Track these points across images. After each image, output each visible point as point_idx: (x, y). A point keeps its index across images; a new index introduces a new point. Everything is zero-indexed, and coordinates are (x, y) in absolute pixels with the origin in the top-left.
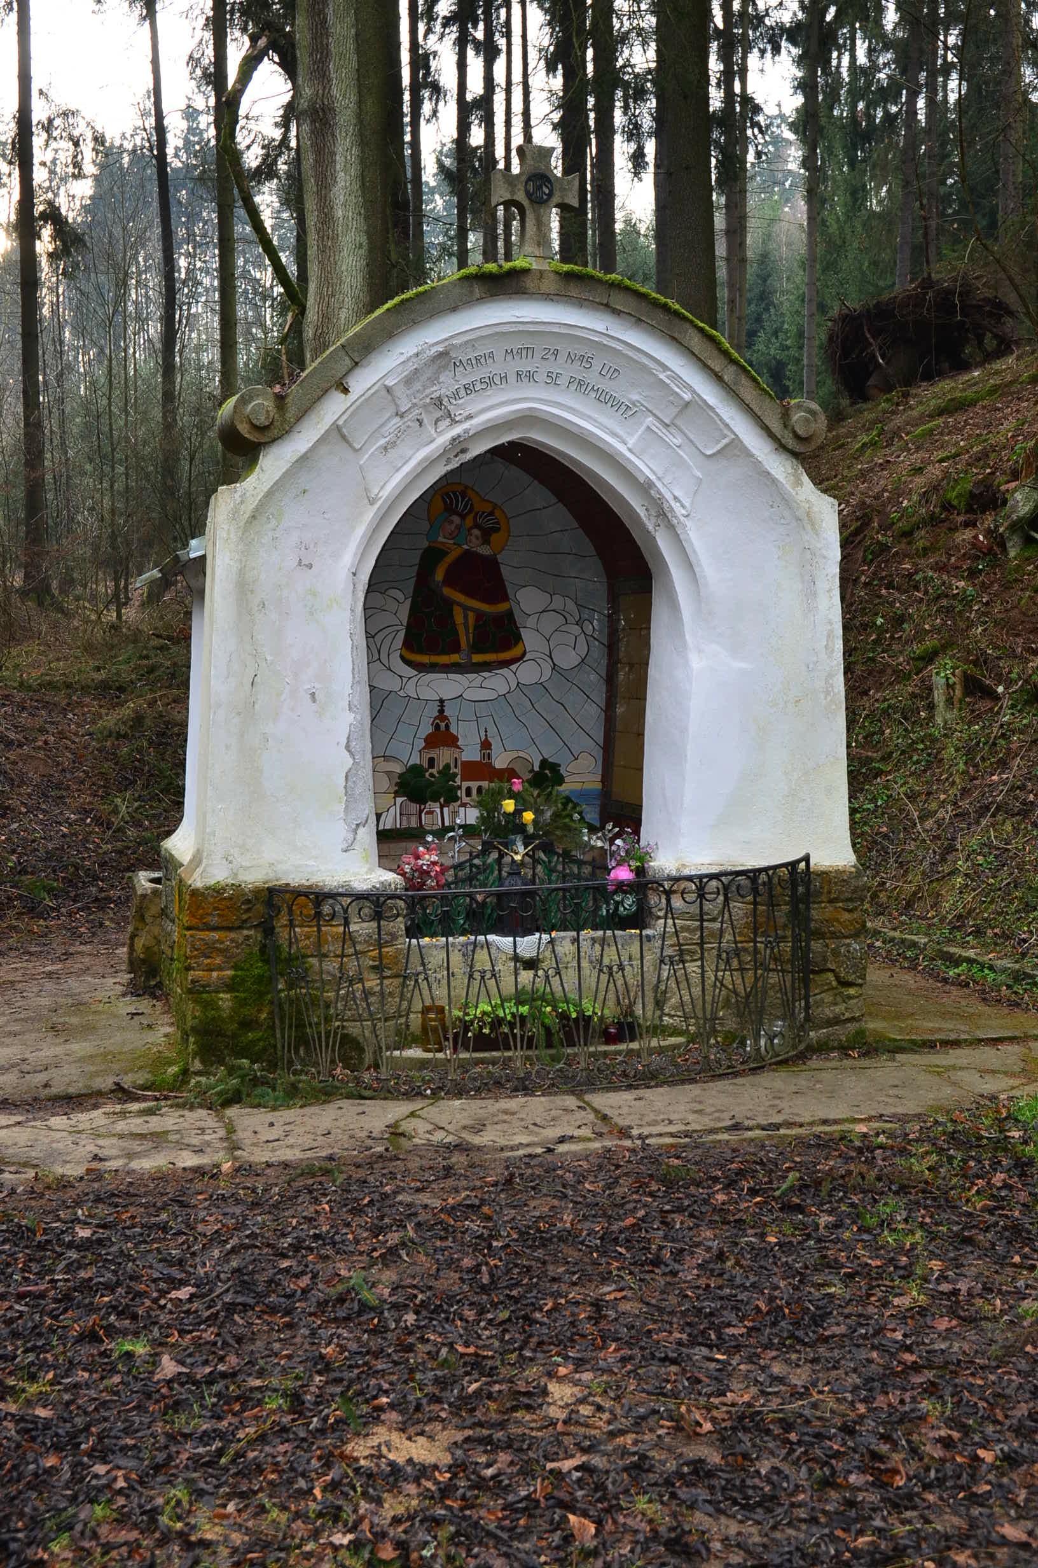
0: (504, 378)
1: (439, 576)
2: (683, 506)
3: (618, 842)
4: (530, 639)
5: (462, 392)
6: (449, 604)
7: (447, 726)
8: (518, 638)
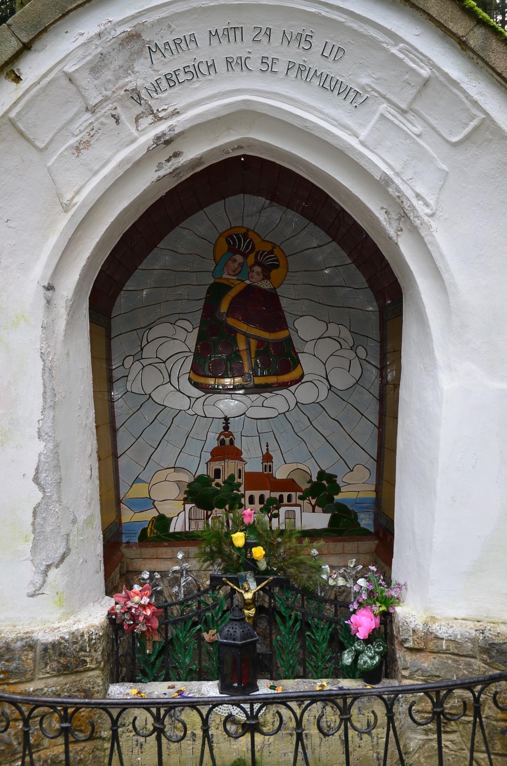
0: (211, 66)
1: (224, 307)
2: (427, 205)
3: (362, 582)
4: (307, 362)
5: (164, 84)
6: (233, 331)
7: (232, 442)
8: (297, 362)
